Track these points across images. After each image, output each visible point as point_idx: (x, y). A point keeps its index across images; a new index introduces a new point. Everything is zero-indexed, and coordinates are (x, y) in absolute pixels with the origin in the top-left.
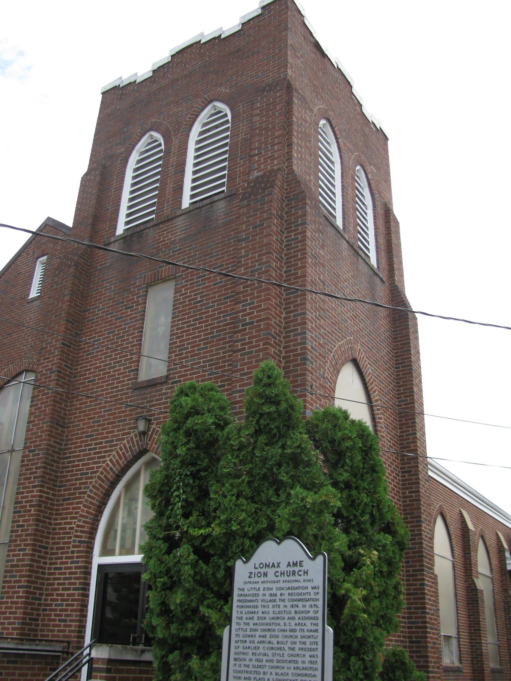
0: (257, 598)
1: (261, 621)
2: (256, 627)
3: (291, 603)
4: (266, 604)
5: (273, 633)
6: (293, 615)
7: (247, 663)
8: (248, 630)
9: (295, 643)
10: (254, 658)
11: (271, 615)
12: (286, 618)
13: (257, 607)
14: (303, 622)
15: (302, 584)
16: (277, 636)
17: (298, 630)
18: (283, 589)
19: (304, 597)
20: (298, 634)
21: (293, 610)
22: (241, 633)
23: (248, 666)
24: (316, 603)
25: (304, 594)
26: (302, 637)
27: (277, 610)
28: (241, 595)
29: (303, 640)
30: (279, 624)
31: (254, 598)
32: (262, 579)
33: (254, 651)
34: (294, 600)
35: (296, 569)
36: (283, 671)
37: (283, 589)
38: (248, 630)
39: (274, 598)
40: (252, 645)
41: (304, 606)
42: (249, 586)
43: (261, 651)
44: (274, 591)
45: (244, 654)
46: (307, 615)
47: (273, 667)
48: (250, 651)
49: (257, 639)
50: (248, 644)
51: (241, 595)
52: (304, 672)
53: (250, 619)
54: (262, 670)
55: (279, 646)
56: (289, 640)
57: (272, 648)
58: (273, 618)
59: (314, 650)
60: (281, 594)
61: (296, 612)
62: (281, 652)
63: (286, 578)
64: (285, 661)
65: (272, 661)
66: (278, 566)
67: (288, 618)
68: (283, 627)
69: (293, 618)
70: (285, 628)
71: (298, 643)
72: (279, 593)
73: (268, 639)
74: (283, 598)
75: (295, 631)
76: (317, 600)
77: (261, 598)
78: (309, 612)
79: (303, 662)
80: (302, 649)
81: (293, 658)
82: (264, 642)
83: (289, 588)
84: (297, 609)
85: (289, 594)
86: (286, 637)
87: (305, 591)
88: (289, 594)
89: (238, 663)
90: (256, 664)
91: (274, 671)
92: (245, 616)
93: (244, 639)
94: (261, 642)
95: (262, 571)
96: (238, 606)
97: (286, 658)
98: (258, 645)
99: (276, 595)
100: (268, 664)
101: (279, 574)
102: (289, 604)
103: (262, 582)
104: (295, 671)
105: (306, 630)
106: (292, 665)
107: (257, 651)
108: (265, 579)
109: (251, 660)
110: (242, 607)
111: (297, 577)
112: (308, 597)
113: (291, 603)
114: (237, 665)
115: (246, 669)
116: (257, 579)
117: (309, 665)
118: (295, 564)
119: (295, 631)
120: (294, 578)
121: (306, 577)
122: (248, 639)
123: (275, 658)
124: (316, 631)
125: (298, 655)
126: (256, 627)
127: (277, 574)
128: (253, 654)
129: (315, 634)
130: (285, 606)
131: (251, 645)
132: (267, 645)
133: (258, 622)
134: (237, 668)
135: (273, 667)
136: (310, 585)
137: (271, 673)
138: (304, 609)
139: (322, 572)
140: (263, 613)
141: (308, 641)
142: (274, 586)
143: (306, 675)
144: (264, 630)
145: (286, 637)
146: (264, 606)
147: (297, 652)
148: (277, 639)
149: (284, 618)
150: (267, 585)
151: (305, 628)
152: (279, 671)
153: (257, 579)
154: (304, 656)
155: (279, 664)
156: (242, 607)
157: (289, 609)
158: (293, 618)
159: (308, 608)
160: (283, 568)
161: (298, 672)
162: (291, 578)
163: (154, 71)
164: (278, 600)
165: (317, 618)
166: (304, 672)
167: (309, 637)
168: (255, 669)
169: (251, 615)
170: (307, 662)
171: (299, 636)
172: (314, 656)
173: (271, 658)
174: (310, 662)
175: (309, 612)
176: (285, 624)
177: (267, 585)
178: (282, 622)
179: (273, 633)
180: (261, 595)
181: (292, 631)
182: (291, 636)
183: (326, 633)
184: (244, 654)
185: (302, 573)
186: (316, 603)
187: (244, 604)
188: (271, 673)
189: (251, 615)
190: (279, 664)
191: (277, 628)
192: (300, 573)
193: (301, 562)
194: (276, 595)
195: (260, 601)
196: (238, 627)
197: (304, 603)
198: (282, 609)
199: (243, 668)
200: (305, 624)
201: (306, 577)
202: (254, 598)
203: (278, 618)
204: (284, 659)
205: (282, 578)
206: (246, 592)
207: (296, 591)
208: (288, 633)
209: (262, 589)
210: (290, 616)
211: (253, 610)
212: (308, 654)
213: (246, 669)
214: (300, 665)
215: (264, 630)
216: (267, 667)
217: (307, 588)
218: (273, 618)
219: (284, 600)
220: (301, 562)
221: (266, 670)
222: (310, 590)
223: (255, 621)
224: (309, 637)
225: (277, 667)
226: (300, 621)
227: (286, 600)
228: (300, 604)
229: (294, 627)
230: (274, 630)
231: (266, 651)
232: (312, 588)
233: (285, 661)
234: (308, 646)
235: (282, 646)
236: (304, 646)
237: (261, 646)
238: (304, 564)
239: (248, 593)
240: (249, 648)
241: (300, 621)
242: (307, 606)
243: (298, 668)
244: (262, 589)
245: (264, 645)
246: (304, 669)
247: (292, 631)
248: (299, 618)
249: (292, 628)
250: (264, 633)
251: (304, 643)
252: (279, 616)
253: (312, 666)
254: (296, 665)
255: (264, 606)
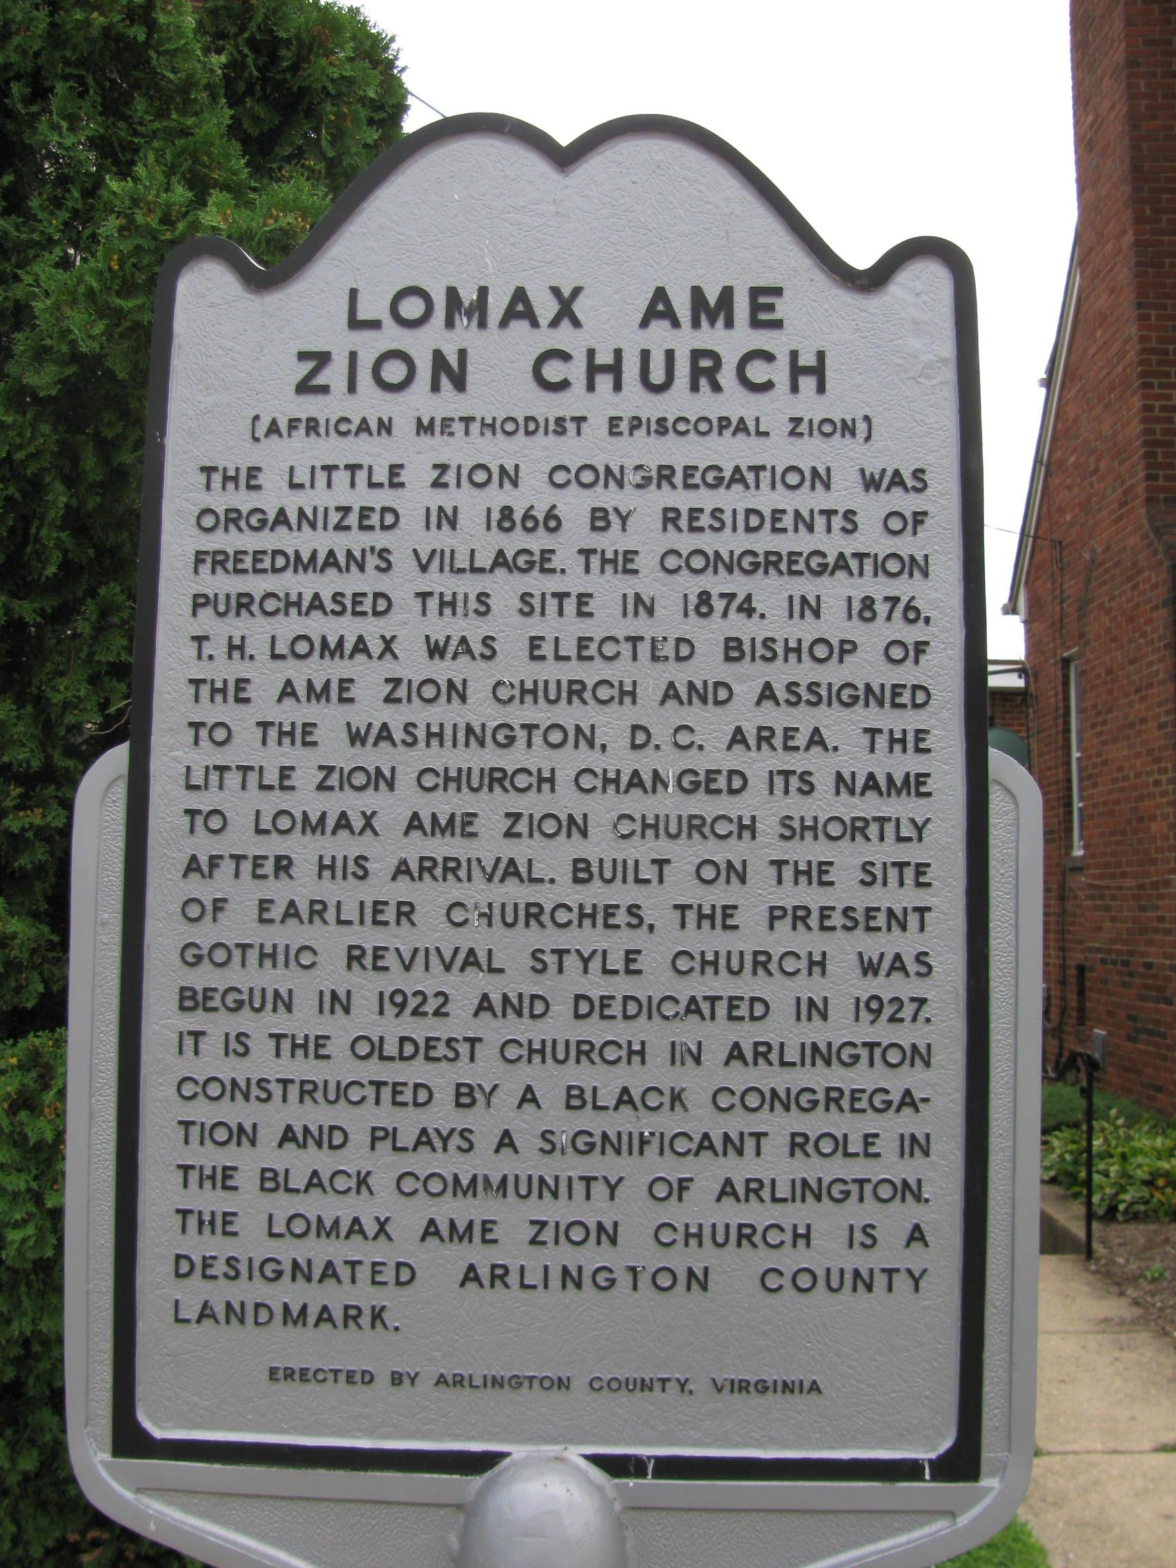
0: (379, 539)
1: (420, 714)
2: (373, 757)
3: (692, 585)
4: (469, 585)
5: (532, 804)
6: (708, 666)
7: (304, 1021)
8: (305, 778)
9: (737, 873)
10: (366, 987)
11: (514, 666)
12: (651, 690)
13: (382, 604)
14: (804, 719)
15: (779, 452)
16: (577, 826)
17: (758, 782)
18: (613, 477)
19: (802, 542)
20: (756, 803)
21: (709, 635)
22: (240, 804)
23: (317, 1047)
24: (903, 588)
25: (804, 522)
26: (791, 830)
27: (569, 629)
28: (233, 518)
29: (807, 851)
30: (585, 737)
31: (356, 541)
32: (421, 401)
33: (370, 938)
34: (715, 562)
35: (731, 343)
36: (636, 1078)
37: (613, 477)
38: (305, 778)
39: (538, 542)
40: (348, 895)
41: (810, 608)
42: (304, 452)
43: (431, 931)
44: (534, 494)
45: (268, 956)
46: (833, 674)
47: (538, 1052)
48: (330, 941)
49: (385, 851)
50: (304, 886)
51: (233, 518)
52: (820, 1078)
53: (317, 693)
54: (442, 1078)
55: (595, 894)
56: (686, 853)
57: (533, 913)
58: (528, 692)
59: (896, 920)
60: (599, 519)
61: (733, 650)
62: (616, 944)
63: (634, 400)
64: (651, 1008)
65: (530, 1006)
66: (566, 312)
67: (670, 693)
68: (622, 760)
69: (711, 694)
70: (645, 763)
71: (761, 874)
72: (575, 506)
73: (489, 845)
74: (612, 541)
75: (737, 783)
76: (916, 567)
77: (410, 537)
78: (847, 648)
79: (816, 1010)
80: (800, 917)
81: (722, 985)
82: (451, 867)
83: (665, 475)
84: (738, 626)
85: (670, 517)
86: (651, 827)
87: (809, 500)
88: (670, 517)
89: (218, 1025)
90: (392, 1028)
91: (551, 1081)
92: (266, 679)
93: (274, 846)
94: (427, 867)
95: (420, 345)
96: (200, 602)
97: (655, 981)
98: (403, 890)
99: (552, 521)
100: (494, 1030)
101: (576, 371)
102: (672, 594)
103: (424, 428)
104: (740, 1077)
105: (824, 782)
106: (717, 1035)
107: (398, 938)
108: (448, 403)
109: (339, 1003)
110: (244, 603)
111: (733, 402)
112: (834, 544)
113: (692, 585)
114: (212, 1045)
115: (302, 1068)
116: (370, 403)
117: (866, 1032)
118: (712, 309)
119: (737, 783)
120: (706, 404)
121: (809, 405)
122: (305, 850)
123: (561, 988)
124: (916, 785)
125: (761, 962)
126: (373, 757)
127: (553, 371)
128: (354, 956)
129: (902, 808)
130: (643, 606)
131: (330, 891)
132: (477, 893)
133: (396, 718)
134: (212, 1062)
135: (538, 1052)
136: (844, 459)
137: (529, 1097)
138: (806, 630)
139: (949, 374)
140: (436, 651)
141: (847, 858)
142: (531, 457)
143: (833, 1098)
144: (454, 780)
145: (651, 827)
146: (448, 604)
147: (752, 934)
148: (574, 848)
149: (629, 694)
150: (460, 451)
151: (822, 766)
152: (606, 1082)
153: (370, 403)
154: (818, 964)
155: (595, 1030)
156: (244, 603)
157: (669, 622)
158: (711, 694)
159: (834, 625)
160: (611, 323)
161: (768, 1077)
162: (680, 402)
163: (390, 64)
164: (565, 557)
165: (920, 697)
166: (820, 1078)
167: (857, 829)
168: (374, 1070)
169: (322, 670)
170: (841, 1010)
171: (768, 826)
172: (898, 965)
173: (519, 982)
174: (873, 1007)
175: (847, 648)
176: (640, 737)
177: (460, 451)
178: (612, 724)
179: (532, 804)
180: (412, 520)
181: (706, 783)
182: (696, 826)
183: (997, 801)
184: (268, 956)
185: (779, 373)
186: (903, 588)
187: (256, 585)
188: (529, 1097)
189: (322, 670)
190: (595, 1030)
191: (568, 762)
192: (757, 372)
193: (763, 301)
194: (552, 521)
195: (403, 562)
196: (208, 755)
197: (806, 586)
198: (607, 619)
199: (262, 1063)
200: (816, 739)
201: (809, 405)
202: (356, 541)
203: (576, 691)
204: (639, 988)
205: (602, 403)
206: (273, 496)
207: (733, 500)
208: (670, 803)
209: (418, 475)
210: (681, 675)
211: (348, 628)
212: (844, 949)
213: (302, 1068)
214: (781, 1028)
215: (454, 780)
216: (487, 1053)
217: (822, 479)
218: (528, 692)
219: (625, 563)
220: (763, 301)
221: (482, 1070)
222: (845, 493)
223: (369, 708)
224: (857, 829)
225: (584, 1051)
226: (777, 718)
227: (647, 562)
228: (771, 592)
229: (718, 757)
230: (547, 781)
231: (477, 937)
232: (871, 483)
233: (651, 1008)
234: (846, 891)
235: (622, 894)
236: (813, 897)
237: (430, 897)
238: (783, 309)
239: (293, 503)
240: (318, 910)
241: (777, 718)
242: (833, 608)
243: (762, 1052)
244: (418, 475)
245: (453, 890)
246: (817, 1054)
247: (706, 783)
248: (767, 693)
249: (700, 763)
250: (447, 804)
251: (819, 874)
252: (590, 673)
253: (883, 1033)
254: (747, 1034)
255: (448, 604)
